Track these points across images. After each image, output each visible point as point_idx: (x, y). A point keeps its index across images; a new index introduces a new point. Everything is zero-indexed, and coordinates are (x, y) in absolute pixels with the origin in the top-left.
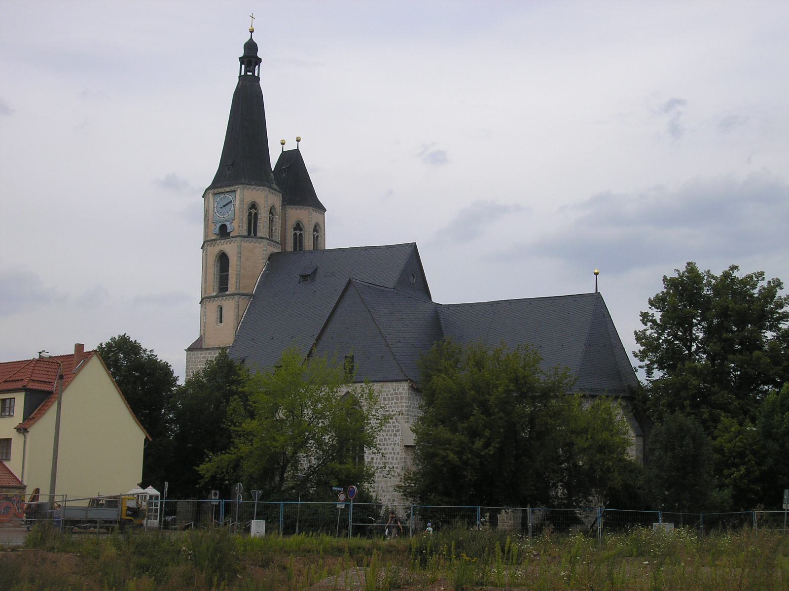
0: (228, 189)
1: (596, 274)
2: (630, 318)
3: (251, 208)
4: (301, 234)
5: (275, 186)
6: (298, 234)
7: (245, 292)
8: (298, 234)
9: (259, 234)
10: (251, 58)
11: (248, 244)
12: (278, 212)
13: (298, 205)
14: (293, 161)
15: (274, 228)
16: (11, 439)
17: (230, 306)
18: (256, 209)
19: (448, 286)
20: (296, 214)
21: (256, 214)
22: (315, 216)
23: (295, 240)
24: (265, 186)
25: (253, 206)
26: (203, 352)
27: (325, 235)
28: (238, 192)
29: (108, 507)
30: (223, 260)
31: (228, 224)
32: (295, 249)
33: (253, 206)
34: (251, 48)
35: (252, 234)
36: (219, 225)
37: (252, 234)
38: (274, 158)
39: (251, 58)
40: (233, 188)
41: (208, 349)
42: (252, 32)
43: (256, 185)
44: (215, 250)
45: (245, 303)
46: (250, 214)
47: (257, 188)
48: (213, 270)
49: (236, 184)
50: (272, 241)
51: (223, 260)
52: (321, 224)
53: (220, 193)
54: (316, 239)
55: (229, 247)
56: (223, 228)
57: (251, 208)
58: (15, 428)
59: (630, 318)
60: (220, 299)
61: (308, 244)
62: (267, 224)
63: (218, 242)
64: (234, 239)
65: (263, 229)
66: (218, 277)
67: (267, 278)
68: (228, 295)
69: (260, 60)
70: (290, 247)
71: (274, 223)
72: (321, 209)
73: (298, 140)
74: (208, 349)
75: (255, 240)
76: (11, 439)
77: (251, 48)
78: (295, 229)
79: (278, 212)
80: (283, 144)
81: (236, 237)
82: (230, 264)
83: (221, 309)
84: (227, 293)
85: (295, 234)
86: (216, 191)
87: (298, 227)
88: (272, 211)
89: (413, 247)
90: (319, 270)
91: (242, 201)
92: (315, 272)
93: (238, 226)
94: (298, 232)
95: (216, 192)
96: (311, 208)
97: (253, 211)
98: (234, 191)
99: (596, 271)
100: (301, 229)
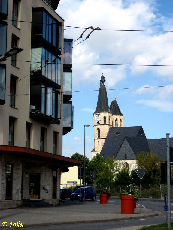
0: (99, 114)
5: (110, 112)
7: (104, 138)
10: (103, 80)
11: (105, 126)
14: (114, 103)
16: (54, 131)
17: (100, 140)
19: (151, 134)
21: (106, 119)
24: (107, 112)
25: (105, 117)
29: (35, 194)
31: (99, 121)
33: (105, 117)
34: (103, 78)
36: (97, 122)
38: (69, 168)
41: (136, 213)
55: (99, 127)
56: (98, 122)
65: (107, 123)
74: (15, 108)
76: (54, 131)
77: (103, 78)
78: (116, 120)
81: (101, 125)
87: (116, 120)
89: (141, 127)
93: (102, 122)
97: (105, 118)
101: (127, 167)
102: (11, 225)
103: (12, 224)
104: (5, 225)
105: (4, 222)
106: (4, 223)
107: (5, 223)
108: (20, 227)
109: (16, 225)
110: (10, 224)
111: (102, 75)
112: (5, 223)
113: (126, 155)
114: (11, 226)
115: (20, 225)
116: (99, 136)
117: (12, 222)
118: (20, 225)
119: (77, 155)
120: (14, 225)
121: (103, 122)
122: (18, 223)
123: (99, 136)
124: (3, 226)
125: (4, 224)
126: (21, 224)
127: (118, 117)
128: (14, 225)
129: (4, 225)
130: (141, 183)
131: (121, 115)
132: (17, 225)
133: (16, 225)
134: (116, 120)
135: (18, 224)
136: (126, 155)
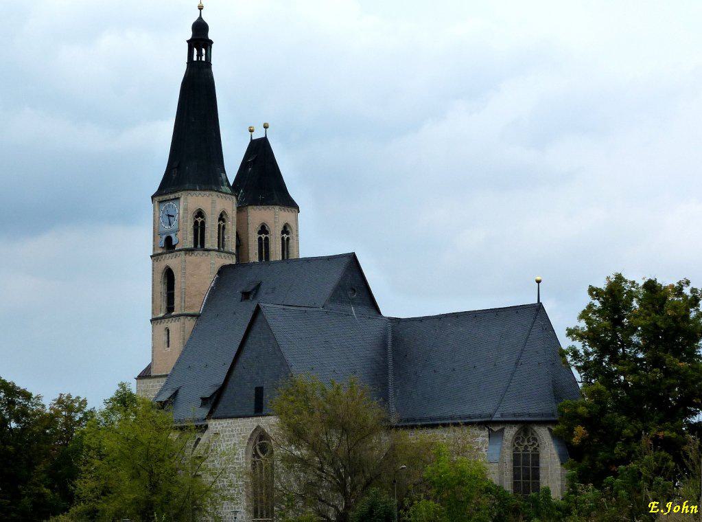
0: (172, 196)
1: (538, 282)
3: (197, 217)
4: (267, 239)
6: (263, 238)
7: (191, 312)
8: (263, 238)
9: (207, 246)
10: (200, 37)
12: (231, 217)
13: (261, 205)
15: (226, 237)
17: (174, 325)
18: (202, 217)
20: (258, 215)
21: (203, 223)
25: (200, 214)
26: (152, 380)
27: (297, 236)
28: (182, 199)
30: (169, 275)
31: (173, 235)
32: (261, 258)
33: (200, 214)
34: (200, 28)
35: (199, 246)
36: (164, 237)
37: (199, 246)
39: (200, 37)
40: (177, 195)
42: (201, 8)
43: (201, 190)
45: (190, 324)
46: (196, 223)
47: (203, 193)
48: (162, 288)
49: (180, 191)
50: (222, 252)
51: (169, 275)
52: (292, 224)
53: (165, 201)
54: (285, 244)
55: (172, 261)
57: (197, 217)
60: (167, 320)
61: (276, 253)
63: (164, 256)
64: (178, 253)
65: (211, 240)
66: (166, 295)
67: (214, 293)
68: (173, 316)
69: (211, 42)
70: (254, 256)
71: (226, 231)
73: (266, 127)
75: (201, 253)
77: (200, 28)
78: (260, 233)
79: (231, 217)
80: (251, 131)
81: (180, 250)
82: (176, 282)
83: (168, 331)
84: (173, 313)
85: (260, 239)
86: (161, 198)
87: (263, 230)
88: (222, 218)
90: (262, 287)
91: (186, 209)
92: (257, 288)
93: (185, 238)
94: (263, 236)
95: (161, 200)
96: (277, 208)
98: (178, 198)
99: (539, 278)
100: (267, 233)
101: (263, 453)
102: (669, 509)
103: (670, 506)
104: (655, 509)
105: (654, 503)
106: (652, 505)
107: (656, 505)
108: (688, 513)
109: (681, 510)
110: (667, 506)
111: (195, 18)
112: (656, 505)
113: (259, 392)
114: (669, 511)
115: (689, 509)
116: (170, 308)
117: (671, 503)
118: (689, 509)
119: (31, 394)
120: (675, 508)
121: (190, 237)
122: (685, 504)
123: (170, 308)
124: (651, 511)
125: (653, 507)
126: (692, 507)
127: (273, 217)
128: (675, 508)
129: (652, 509)
130: (531, 476)
131: (291, 204)
132: (683, 510)
133: (681, 510)
134: (263, 230)
135: (684, 507)
136: (259, 392)
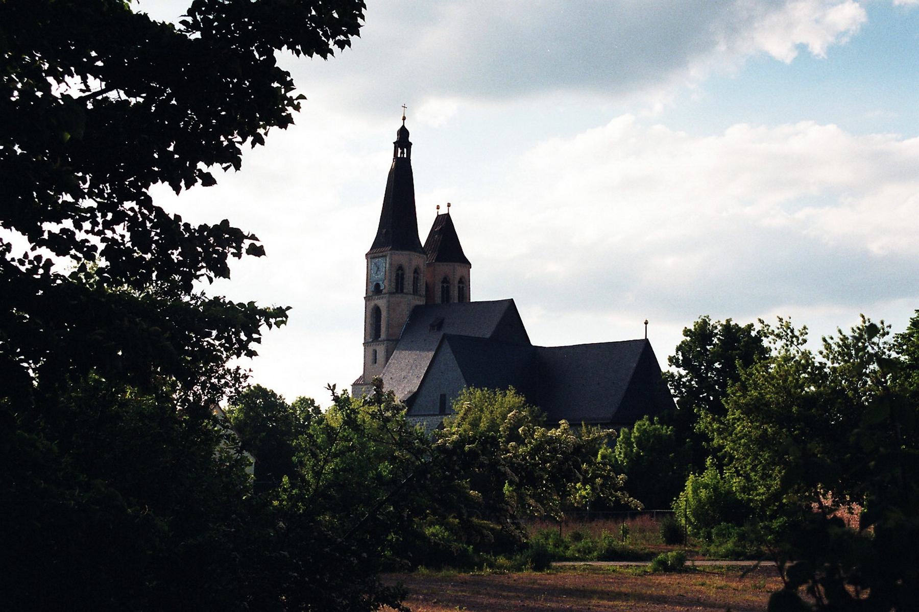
2: (666, 347)
10: (403, 140)
20: (444, 268)
21: (403, 274)
22: (459, 269)
23: (443, 292)
25: (400, 268)
31: (381, 283)
32: (443, 301)
34: (403, 133)
39: (403, 140)
44: (373, 304)
55: (382, 303)
58: (253, 147)
59: (666, 347)
62: (411, 283)
70: (438, 300)
72: (467, 264)
77: (403, 133)
78: (443, 282)
85: (443, 287)
87: (445, 280)
89: (511, 302)
97: (400, 272)
98: (386, 256)
